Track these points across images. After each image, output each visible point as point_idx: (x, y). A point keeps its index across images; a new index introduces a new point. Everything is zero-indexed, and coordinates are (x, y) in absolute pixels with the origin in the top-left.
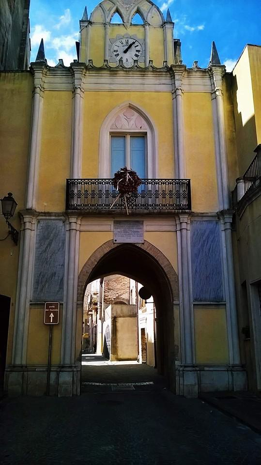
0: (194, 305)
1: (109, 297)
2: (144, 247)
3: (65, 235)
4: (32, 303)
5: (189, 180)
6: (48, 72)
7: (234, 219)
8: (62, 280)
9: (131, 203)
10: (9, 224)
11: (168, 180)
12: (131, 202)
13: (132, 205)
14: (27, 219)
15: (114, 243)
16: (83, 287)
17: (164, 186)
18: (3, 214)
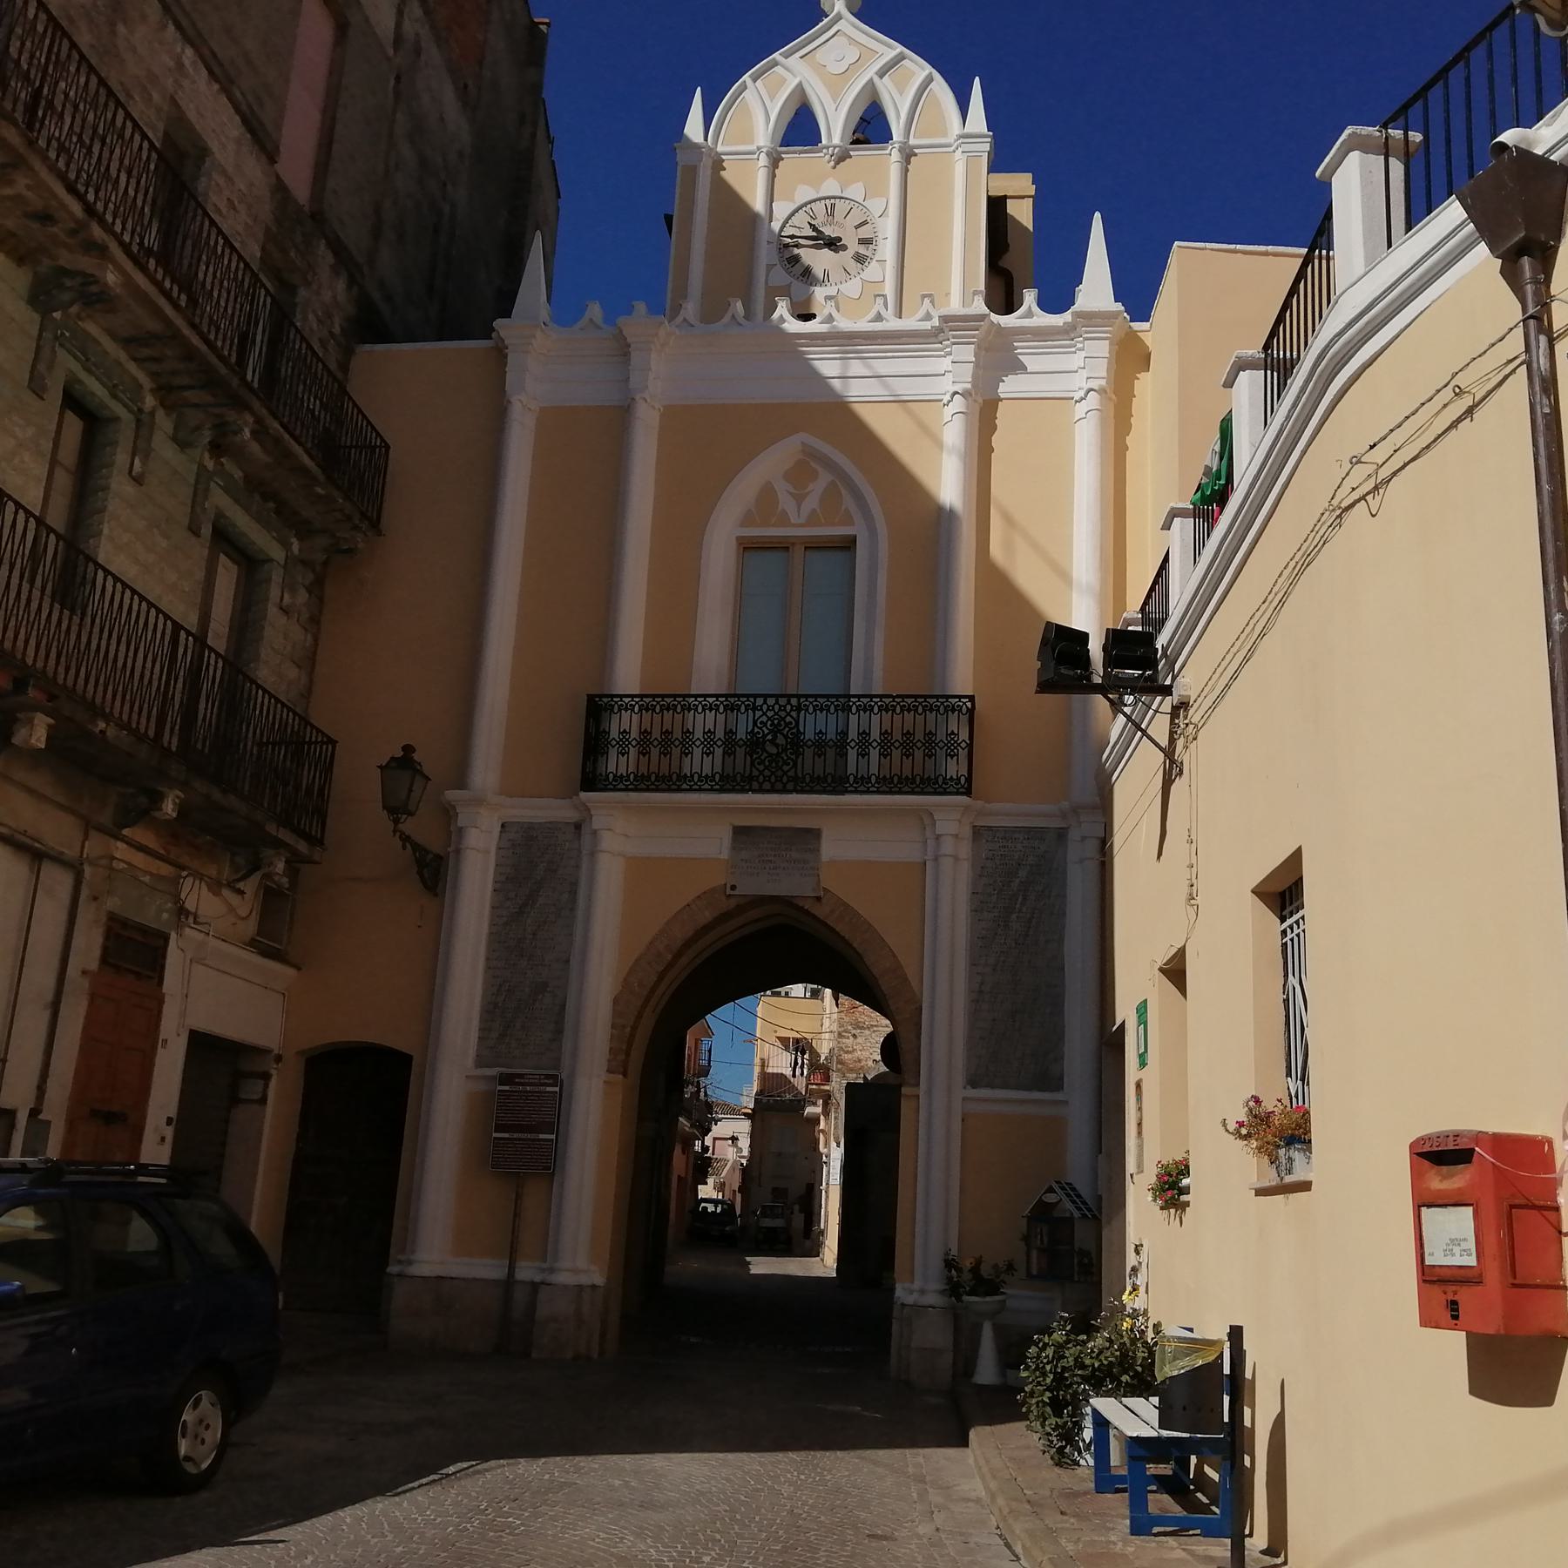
0: (964, 1099)
2: (820, 911)
5: (971, 698)
9: (770, 714)
10: (406, 839)
12: (769, 719)
13: (765, 707)
17: (909, 717)
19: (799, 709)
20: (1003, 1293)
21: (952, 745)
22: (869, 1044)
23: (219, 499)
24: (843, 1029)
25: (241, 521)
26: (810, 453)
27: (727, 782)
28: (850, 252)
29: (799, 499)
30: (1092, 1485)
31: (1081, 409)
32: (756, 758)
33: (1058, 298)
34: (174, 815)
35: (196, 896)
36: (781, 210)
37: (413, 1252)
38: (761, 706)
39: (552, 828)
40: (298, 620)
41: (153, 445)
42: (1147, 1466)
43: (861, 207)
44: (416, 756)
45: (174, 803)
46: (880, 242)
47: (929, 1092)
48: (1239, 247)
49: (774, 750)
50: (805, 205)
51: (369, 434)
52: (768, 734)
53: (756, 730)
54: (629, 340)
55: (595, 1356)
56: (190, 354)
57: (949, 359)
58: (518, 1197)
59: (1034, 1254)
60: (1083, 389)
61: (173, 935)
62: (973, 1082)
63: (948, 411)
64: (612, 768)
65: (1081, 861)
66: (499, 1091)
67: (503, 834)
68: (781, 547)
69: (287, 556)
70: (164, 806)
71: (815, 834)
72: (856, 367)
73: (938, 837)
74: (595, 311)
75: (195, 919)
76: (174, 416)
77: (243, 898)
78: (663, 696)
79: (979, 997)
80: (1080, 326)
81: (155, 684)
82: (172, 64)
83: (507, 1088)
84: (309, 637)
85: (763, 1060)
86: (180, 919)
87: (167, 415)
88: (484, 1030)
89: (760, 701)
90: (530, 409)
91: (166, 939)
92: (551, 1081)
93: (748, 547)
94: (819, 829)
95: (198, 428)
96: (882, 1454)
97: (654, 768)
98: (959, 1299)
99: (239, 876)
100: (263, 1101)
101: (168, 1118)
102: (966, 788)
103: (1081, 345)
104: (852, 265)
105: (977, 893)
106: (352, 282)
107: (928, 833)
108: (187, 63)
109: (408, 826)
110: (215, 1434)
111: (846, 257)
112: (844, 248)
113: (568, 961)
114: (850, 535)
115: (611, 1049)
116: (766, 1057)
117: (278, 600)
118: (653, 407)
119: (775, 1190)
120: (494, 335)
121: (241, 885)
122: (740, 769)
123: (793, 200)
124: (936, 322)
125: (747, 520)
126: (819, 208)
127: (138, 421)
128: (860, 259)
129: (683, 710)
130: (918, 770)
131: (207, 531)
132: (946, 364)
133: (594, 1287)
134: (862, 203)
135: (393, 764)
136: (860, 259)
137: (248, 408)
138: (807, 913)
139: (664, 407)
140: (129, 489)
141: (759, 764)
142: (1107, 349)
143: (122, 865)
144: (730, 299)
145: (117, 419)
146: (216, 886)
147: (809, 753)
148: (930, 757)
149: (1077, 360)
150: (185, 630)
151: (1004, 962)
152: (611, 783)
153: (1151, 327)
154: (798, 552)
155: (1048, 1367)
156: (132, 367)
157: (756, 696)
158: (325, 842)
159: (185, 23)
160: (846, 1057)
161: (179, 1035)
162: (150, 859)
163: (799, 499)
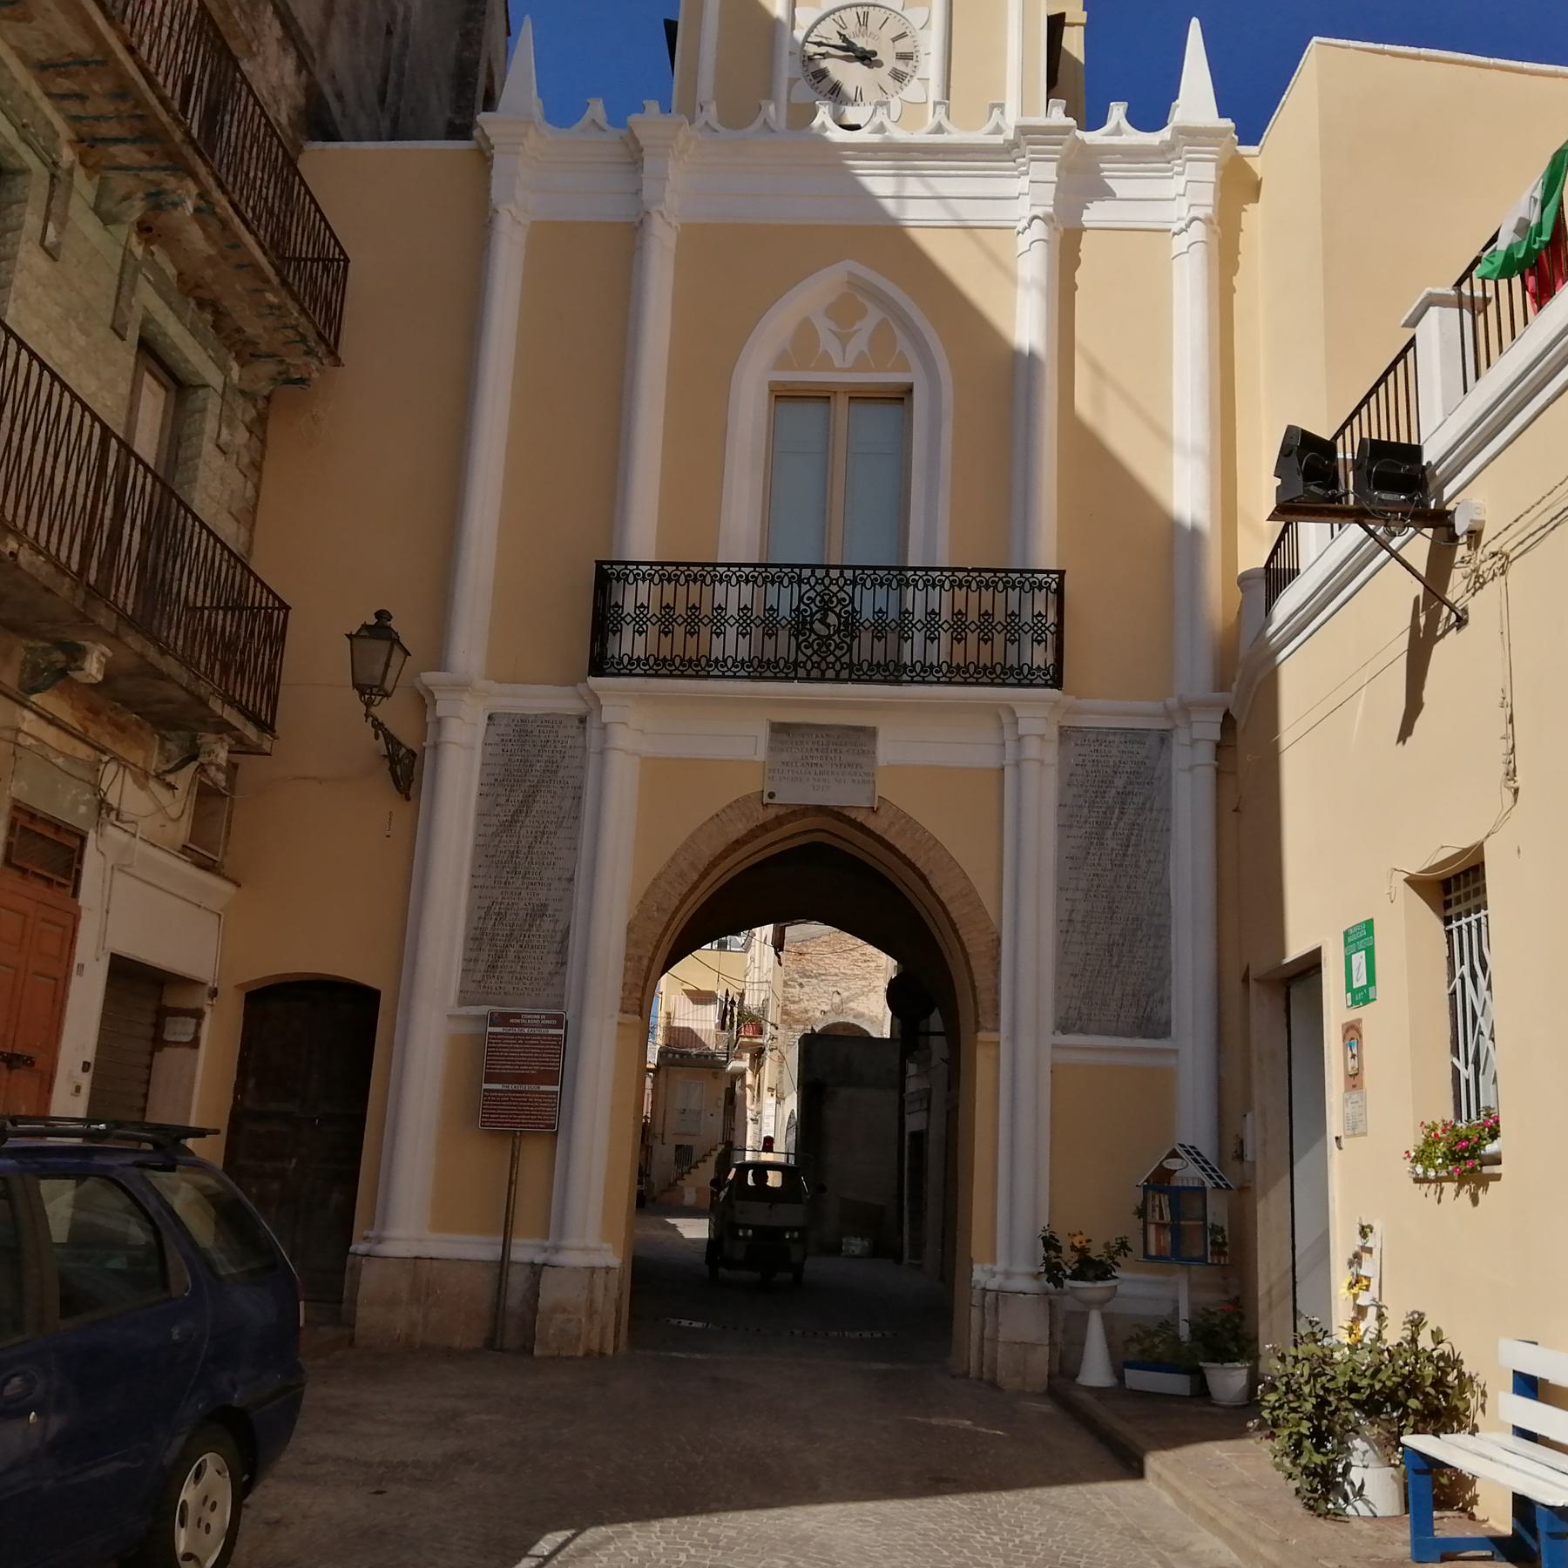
0: (1054, 1047)
5: (1061, 573)
9: (831, 659)
10: (378, 725)
11: (875, 568)
12: (818, 594)
16: (645, 962)
17: (987, 595)
18: (356, 685)
19: (854, 583)
20: (1116, 1278)
22: (816, 994)
23: (147, 298)
25: (175, 332)
26: (855, 283)
27: (760, 669)
28: (886, 69)
29: (844, 340)
30: (1408, 1549)
31: (1180, 243)
32: (802, 642)
33: (1150, 115)
34: (100, 678)
35: (121, 788)
36: (805, 17)
37: (384, 1225)
38: (808, 579)
39: (550, 722)
40: (237, 464)
41: (70, 214)
42: (1435, 1514)
43: (899, 17)
44: (393, 624)
45: (99, 661)
46: (922, 57)
47: (1013, 1038)
48: (1387, 47)
49: (823, 631)
50: (833, 12)
51: (327, 240)
52: (817, 612)
53: (848, 640)
54: (642, 143)
55: (610, 1352)
56: (123, 91)
57: (1026, 179)
58: (514, 1160)
59: (1152, 1229)
60: (1183, 219)
61: (92, 836)
62: (1064, 1027)
63: (1023, 242)
64: (626, 649)
65: (1191, 768)
67: (491, 727)
68: (822, 396)
69: (225, 383)
70: (87, 665)
71: (870, 733)
72: (913, 186)
73: (1020, 739)
74: (597, 109)
75: (117, 815)
76: (97, 179)
78: (689, 565)
79: (1067, 926)
80: (1182, 144)
81: (80, 500)
83: (499, 1030)
84: (250, 485)
85: (668, 1014)
86: (100, 814)
87: (90, 178)
88: (469, 963)
89: (806, 573)
90: (519, 223)
91: (83, 839)
92: (555, 1022)
93: (783, 396)
94: (875, 728)
95: (127, 197)
96: (1055, 1493)
97: (678, 650)
98: (1058, 1283)
99: (171, 766)
100: (194, 1043)
101: (85, 1063)
102: (1056, 679)
103: (1181, 169)
104: (890, 83)
105: (1065, 806)
106: (302, 64)
107: (1008, 734)
109: (382, 710)
110: (220, 1519)
111: (882, 74)
112: (880, 64)
113: (571, 880)
115: (624, 984)
116: (671, 1010)
117: (215, 436)
118: (670, 224)
119: (678, 1147)
120: (476, 133)
121: (170, 778)
122: (782, 652)
123: (817, 5)
124: (1010, 134)
125: (782, 361)
126: (850, 17)
127: (53, 176)
128: (898, 76)
130: (998, 658)
131: (133, 335)
132: (1022, 184)
133: (608, 1269)
134: (900, 12)
135: (364, 633)
136: (898, 76)
137: (194, 176)
138: (862, 828)
139: (683, 225)
140: (40, 262)
141: (806, 647)
142: (1213, 172)
143: (30, 741)
144: (763, 102)
145: (25, 171)
146: (142, 777)
147: (866, 637)
149: (1176, 185)
150: (117, 438)
151: (1098, 886)
153: (1260, 152)
154: (841, 404)
155: (1306, 1389)
156: (47, 107)
157: (801, 567)
158: (276, 728)
160: (792, 1007)
161: (97, 960)
162: (64, 737)
163: (844, 340)
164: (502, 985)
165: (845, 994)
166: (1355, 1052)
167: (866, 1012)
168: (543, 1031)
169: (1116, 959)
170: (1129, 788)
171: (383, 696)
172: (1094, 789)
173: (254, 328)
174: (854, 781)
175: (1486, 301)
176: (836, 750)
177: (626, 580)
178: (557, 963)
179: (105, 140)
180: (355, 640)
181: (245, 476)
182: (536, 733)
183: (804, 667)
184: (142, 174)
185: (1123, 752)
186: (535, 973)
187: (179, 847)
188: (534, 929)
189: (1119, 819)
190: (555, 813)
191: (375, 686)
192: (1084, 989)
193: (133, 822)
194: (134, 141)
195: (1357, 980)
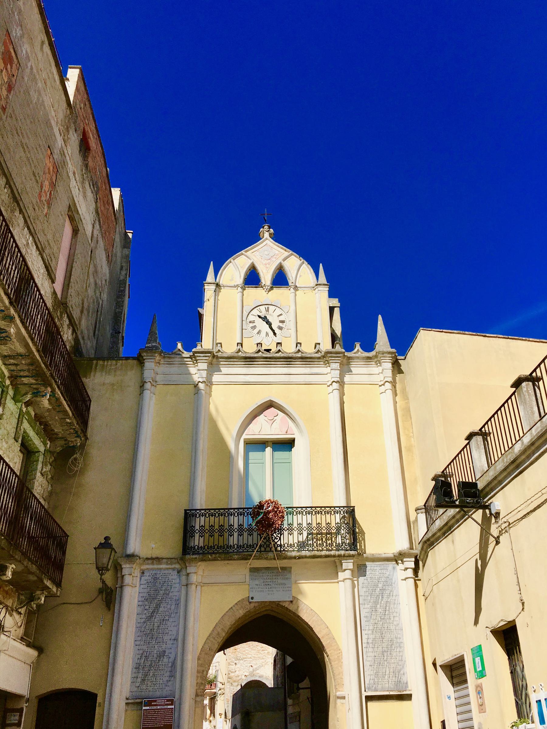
1: (237, 673)
3: (179, 591)
4: (130, 701)
6: (162, 360)
7: (417, 563)
8: (174, 664)
14: (126, 568)
15: (250, 603)
18: (97, 568)
21: (231, 530)
23: (26, 425)
24: (230, 661)
33: (369, 346)
40: (46, 479)
53: (279, 535)
66: (144, 710)
70: (7, 573)
77: (20, 616)
78: (219, 509)
82: (25, 243)
83: (148, 708)
92: (170, 703)
106: (74, 331)
108: (30, 242)
114: (292, 438)
129: (228, 515)
130: (216, 543)
137: (51, 386)
148: (221, 536)
152: (196, 551)
159: (31, 227)
160: (232, 675)
164: (148, 688)
165: (254, 667)
166: (481, 696)
167: (264, 674)
168: (166, 707)
169: (385, 658)
170: (384, 587)
171: (107, 570)
172: (372, 589)
173: (58, 429)
174: (283, 590)
175: (490, 433)
176: (276, 578)
177: (196, 516)
178: (170, 676)
179: (21, 376)
180: (97, 550)
181: (48, 483)
182: (160, 578)
183: (264, 547)
184: (32, 386)
185: (381, 573)
186: (161, 681)
187: (20, 638)
188: (160, 662)
189: (382, 600)
190: (168, 611)
191: (105, 568)
192: (375, 671)
193: (9, 631)
194: (32, 377)
195: (479, 668)
